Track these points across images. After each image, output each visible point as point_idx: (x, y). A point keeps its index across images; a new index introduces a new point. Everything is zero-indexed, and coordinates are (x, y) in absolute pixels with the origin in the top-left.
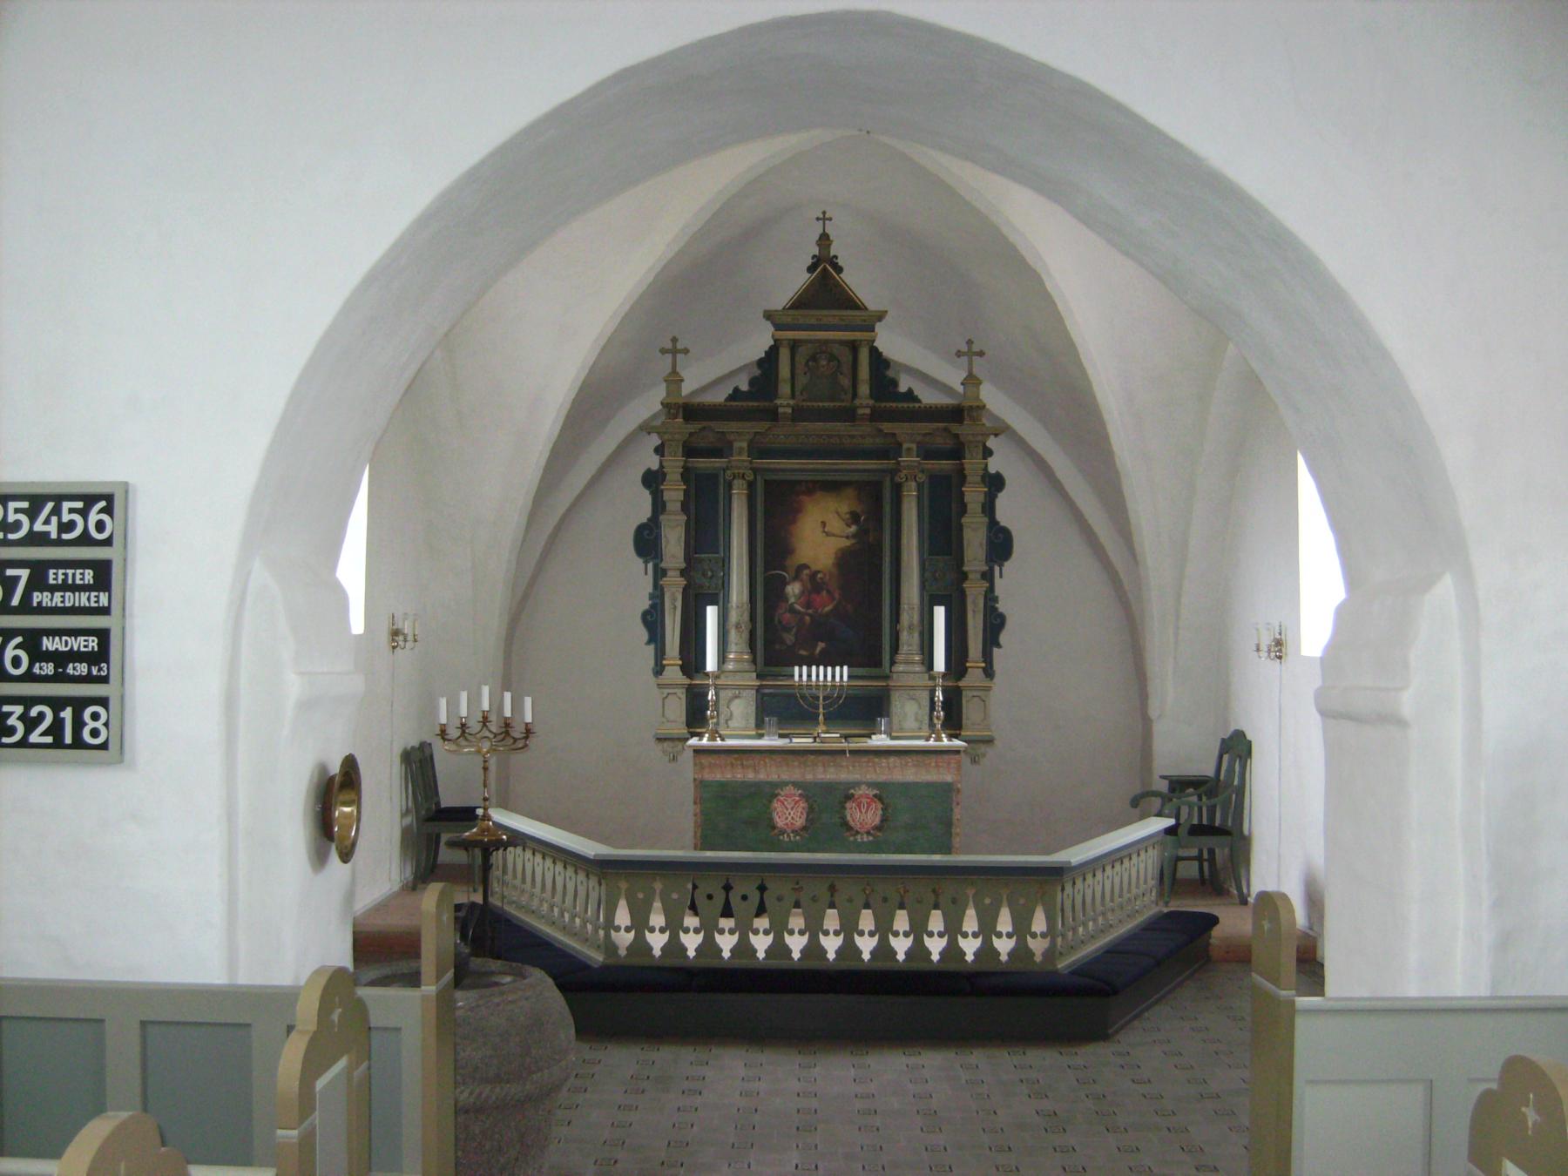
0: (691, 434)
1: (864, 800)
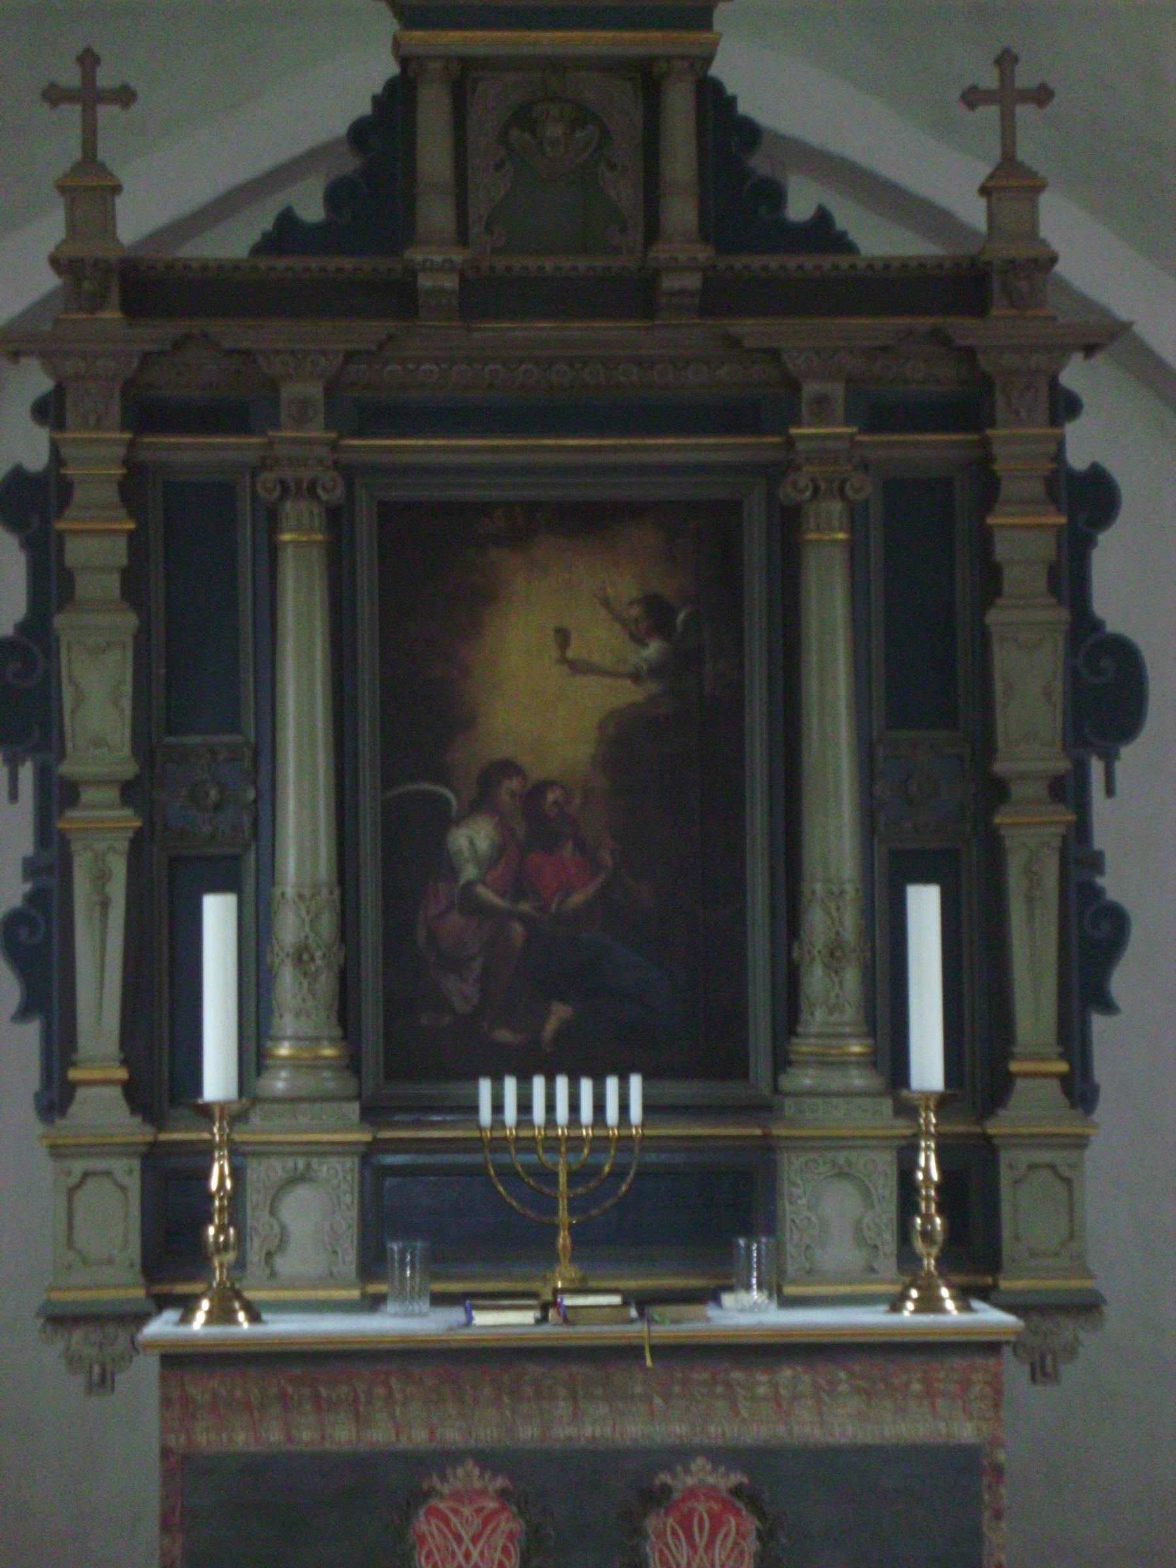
0: (146, 357)
1: (701, 1507)
